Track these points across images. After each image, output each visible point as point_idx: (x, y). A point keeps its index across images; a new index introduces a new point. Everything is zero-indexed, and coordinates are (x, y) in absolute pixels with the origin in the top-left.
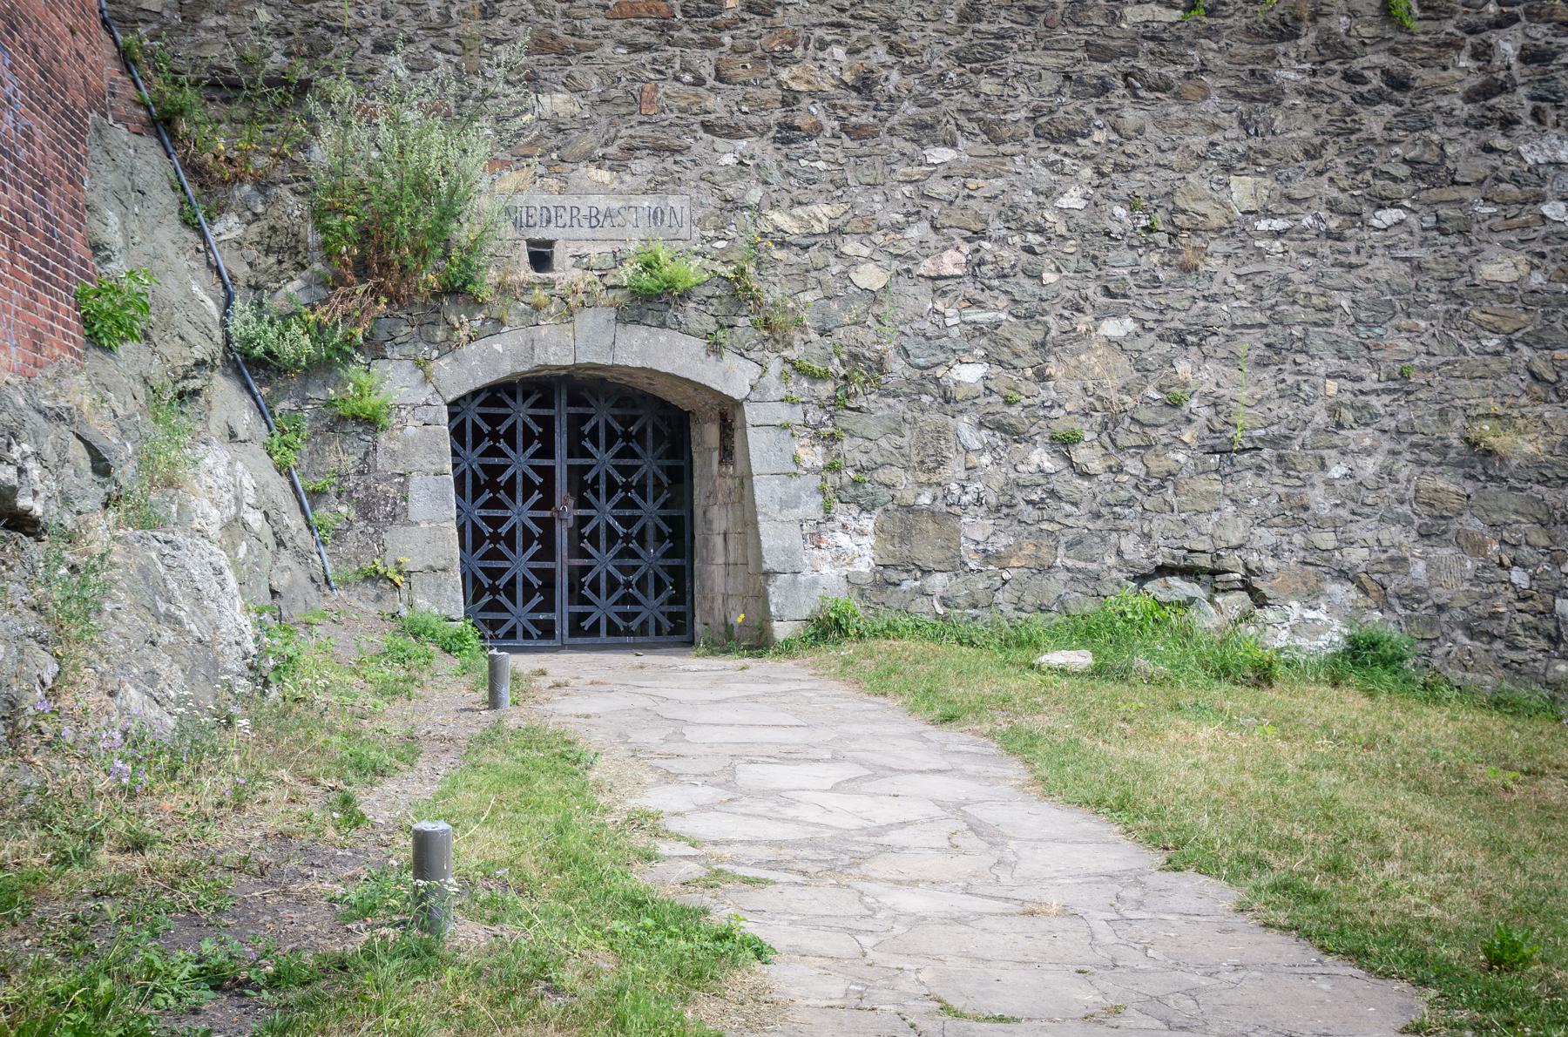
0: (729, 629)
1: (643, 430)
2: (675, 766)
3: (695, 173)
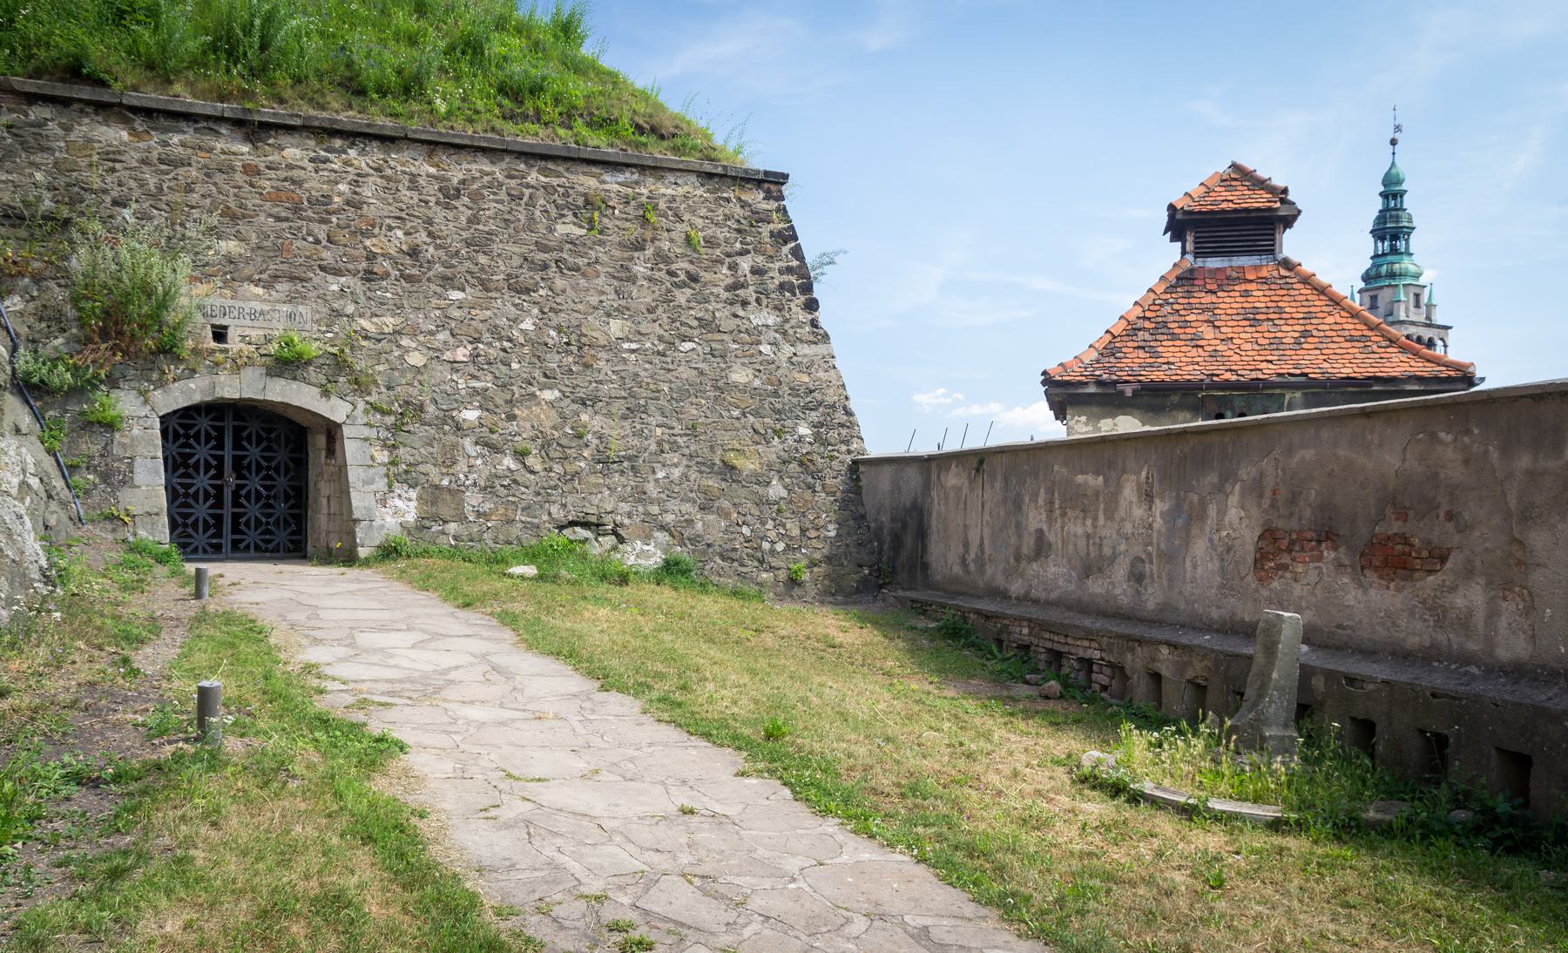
0: (329, 551)
1: (278, 436)
2: (319, 634)
3: (315, 293)
